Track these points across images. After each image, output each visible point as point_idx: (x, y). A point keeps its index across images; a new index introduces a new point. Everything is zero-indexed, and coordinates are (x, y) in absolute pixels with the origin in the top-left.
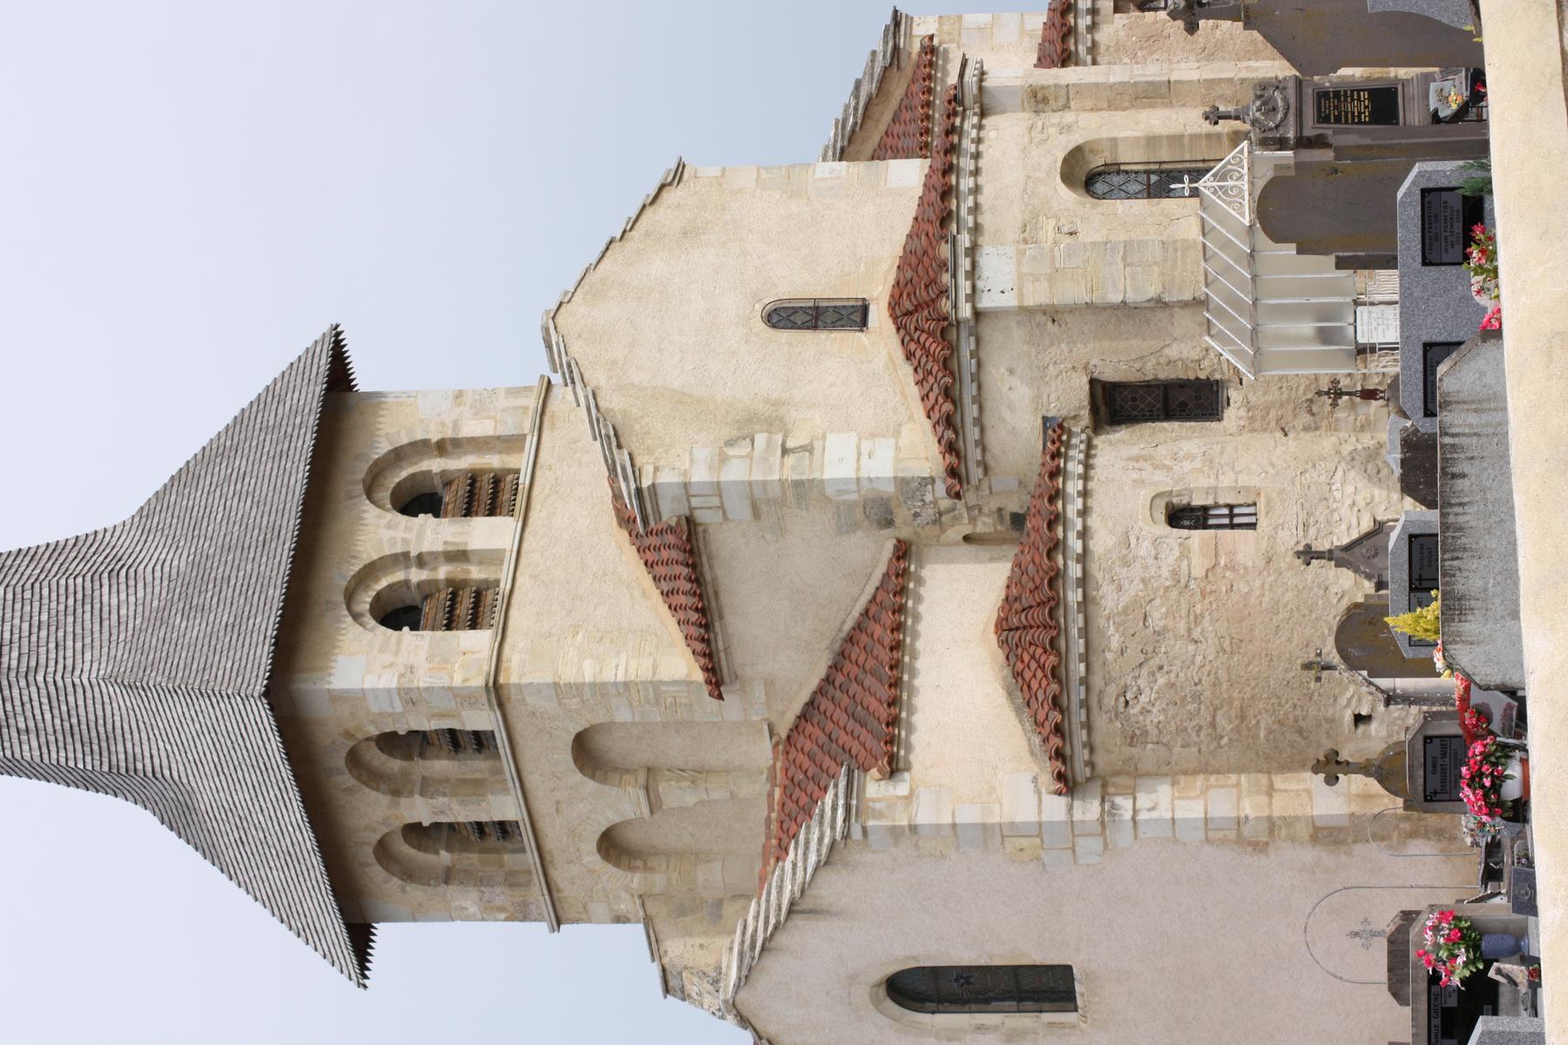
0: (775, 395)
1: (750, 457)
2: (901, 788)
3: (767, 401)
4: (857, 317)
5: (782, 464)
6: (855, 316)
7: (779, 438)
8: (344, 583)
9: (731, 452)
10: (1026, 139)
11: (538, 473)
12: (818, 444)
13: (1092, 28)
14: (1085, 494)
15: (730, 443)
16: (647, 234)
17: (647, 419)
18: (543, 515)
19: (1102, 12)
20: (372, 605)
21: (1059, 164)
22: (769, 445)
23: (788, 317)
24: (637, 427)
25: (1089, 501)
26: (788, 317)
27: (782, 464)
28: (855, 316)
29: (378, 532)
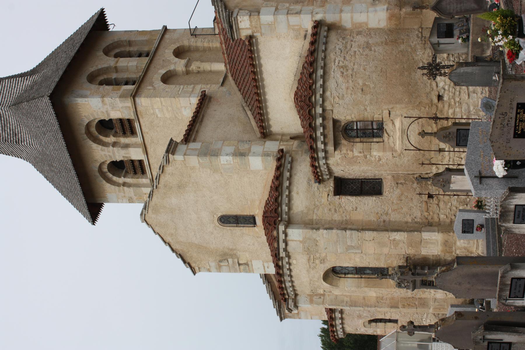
0: (231, 247)
1: (228, 265)
2: (281, 148)
3: (229, 249)
4: (252, 221)
5: (240, 268)
6: (251, 221)
7: (236, 260)
8: (97, 169)
9: (222, 264)
10: (308, 266)
11: (144, 135)
12: (249, 263)
13: (326, 158)
14: (342, 318)
15: (221, 261)
16: (165, 186)
17: (190, 253)
18: (152, 150)
19: (329, 152)
20: (108, 168)
21: (322, 276)
22: (233, 262)
23: (227, 220)
24: (188, 255)
25: (328, 39)
26: (227, 220)
27: (240, 268)
28: (251, 221)
29: (102, 154)
